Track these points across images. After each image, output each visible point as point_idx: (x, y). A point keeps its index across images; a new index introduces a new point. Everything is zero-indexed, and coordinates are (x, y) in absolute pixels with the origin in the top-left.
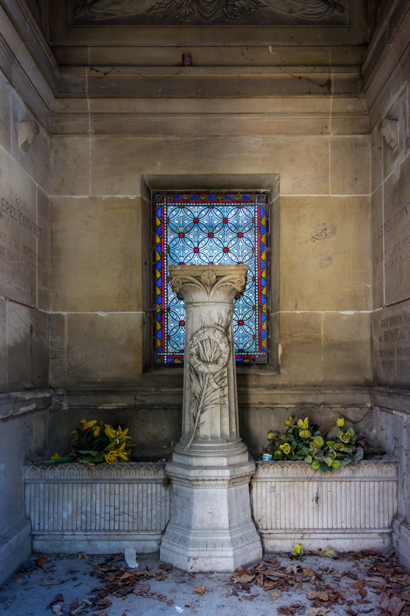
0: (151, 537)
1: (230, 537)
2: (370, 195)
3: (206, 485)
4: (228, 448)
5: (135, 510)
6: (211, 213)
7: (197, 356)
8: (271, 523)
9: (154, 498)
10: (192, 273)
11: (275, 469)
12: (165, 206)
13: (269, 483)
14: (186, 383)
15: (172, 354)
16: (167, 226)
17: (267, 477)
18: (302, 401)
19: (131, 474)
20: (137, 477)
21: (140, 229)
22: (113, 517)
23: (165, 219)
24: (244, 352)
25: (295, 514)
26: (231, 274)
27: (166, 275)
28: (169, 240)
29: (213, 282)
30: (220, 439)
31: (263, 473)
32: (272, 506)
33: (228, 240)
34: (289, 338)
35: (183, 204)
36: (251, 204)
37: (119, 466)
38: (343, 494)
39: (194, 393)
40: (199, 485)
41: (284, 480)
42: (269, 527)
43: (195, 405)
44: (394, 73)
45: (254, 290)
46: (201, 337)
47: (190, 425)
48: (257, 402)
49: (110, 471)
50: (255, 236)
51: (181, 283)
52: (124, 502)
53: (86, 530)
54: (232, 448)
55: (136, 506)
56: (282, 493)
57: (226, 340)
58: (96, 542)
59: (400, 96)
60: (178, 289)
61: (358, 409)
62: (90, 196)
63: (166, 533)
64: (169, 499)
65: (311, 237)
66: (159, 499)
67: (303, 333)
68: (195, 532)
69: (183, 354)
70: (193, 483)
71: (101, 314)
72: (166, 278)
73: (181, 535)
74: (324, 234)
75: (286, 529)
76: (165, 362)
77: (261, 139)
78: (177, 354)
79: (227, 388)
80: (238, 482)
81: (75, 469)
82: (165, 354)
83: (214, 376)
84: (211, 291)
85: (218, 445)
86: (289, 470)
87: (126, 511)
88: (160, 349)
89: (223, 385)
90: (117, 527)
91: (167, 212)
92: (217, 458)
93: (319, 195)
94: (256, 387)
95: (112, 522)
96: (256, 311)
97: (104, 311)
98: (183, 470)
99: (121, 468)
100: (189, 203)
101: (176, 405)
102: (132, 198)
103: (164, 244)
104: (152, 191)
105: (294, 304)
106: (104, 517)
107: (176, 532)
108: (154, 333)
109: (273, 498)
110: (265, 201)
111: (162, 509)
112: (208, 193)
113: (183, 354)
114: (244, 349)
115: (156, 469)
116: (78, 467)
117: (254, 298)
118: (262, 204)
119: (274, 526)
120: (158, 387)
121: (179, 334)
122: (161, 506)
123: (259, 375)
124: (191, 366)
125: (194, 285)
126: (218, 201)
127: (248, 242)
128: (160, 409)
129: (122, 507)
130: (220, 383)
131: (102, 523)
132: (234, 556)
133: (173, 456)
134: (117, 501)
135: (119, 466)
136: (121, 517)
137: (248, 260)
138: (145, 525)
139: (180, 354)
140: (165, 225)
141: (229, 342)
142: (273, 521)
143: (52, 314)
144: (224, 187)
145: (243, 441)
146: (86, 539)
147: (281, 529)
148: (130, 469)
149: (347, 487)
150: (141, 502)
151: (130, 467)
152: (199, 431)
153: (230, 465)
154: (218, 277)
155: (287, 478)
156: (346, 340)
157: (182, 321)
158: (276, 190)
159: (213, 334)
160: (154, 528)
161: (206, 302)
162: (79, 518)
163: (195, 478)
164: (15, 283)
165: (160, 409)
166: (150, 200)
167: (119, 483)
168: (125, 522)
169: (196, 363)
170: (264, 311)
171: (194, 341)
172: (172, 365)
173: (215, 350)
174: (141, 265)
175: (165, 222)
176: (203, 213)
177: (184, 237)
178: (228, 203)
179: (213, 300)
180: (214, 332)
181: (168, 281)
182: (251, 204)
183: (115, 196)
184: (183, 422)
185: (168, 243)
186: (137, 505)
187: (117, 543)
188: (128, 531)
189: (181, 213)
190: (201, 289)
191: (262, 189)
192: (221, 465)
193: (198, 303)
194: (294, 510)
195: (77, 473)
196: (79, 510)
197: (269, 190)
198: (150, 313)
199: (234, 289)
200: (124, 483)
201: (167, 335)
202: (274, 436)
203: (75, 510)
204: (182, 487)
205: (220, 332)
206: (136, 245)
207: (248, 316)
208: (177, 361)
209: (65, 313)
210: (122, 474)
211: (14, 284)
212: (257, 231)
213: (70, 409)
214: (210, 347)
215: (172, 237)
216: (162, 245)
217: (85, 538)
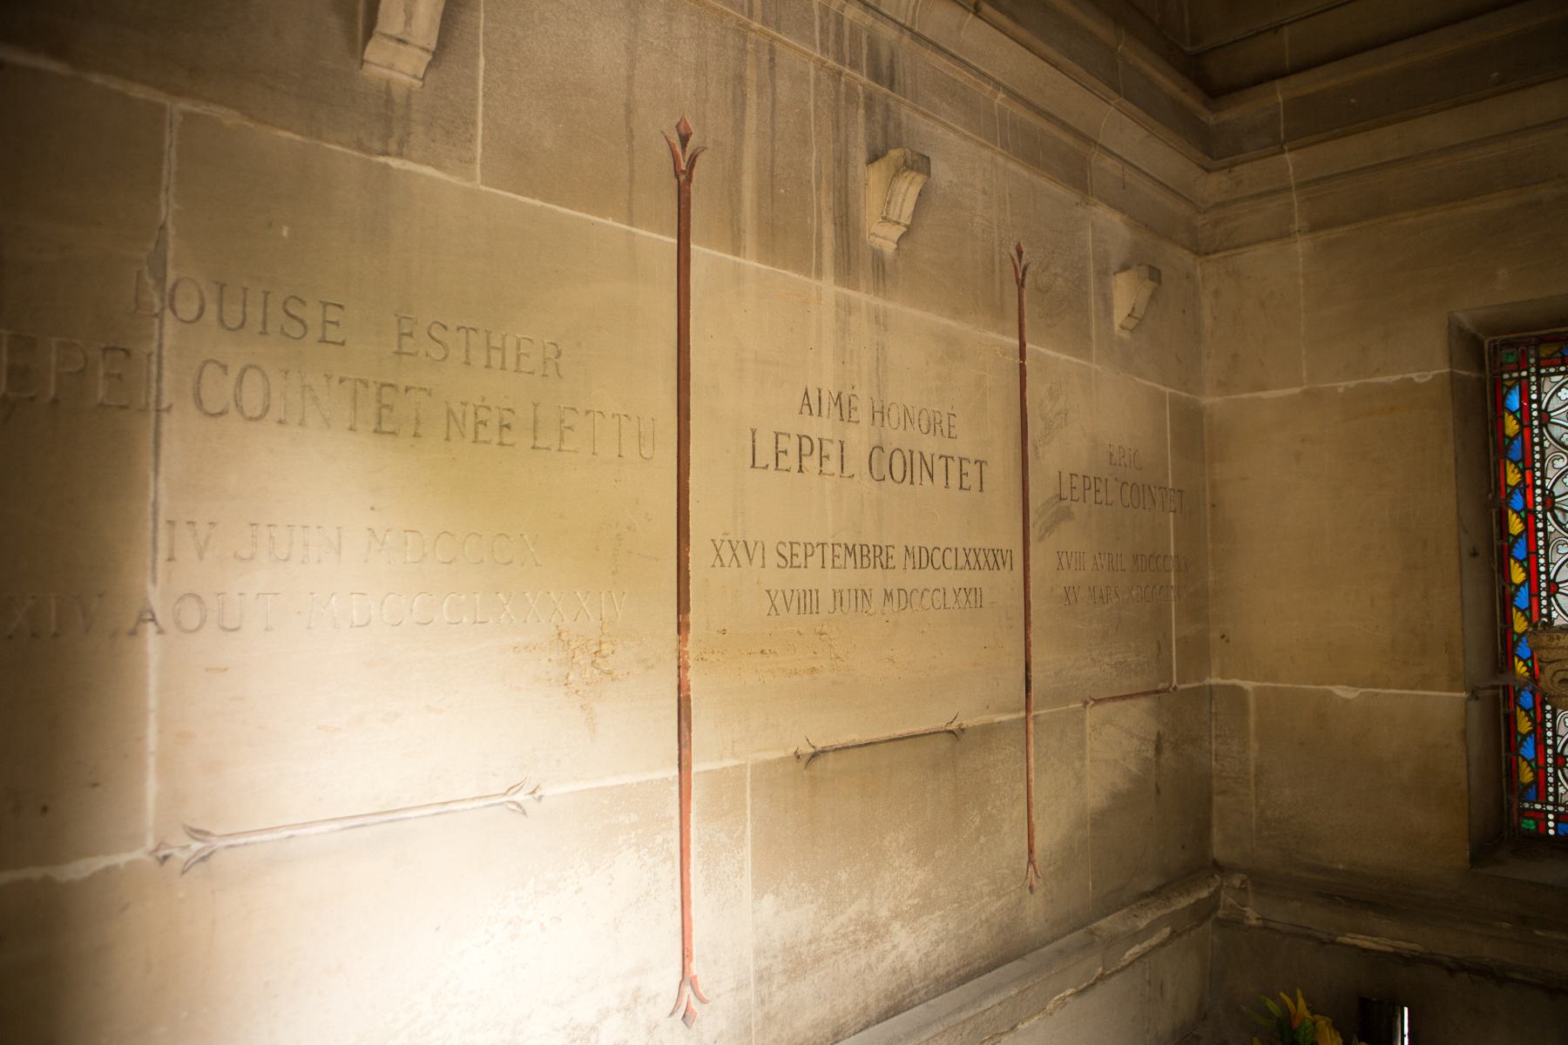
12: (1533, 379)
16: (1541, 435)
23: (1535, 414)
27: (1543, 577)
28: (1551, 473)
71: (1343, 692)
72: (1543, 585)
82: (1550, 808)
88: (1532, 793)
97: (1352, 683)
103: (1536, 487)
104: (1486, 342)
108: (1508, 741)
143: (1218, 686)
164: (1111, 655)
166: (1482, 367)
175: (1536, 423)
183: (1372, 380)
185: (1548, 484)
206: (1441, 504)
209: (1248, 685)
211: (1107, 659)
213: (1265, 928)
215: (1560, 464)
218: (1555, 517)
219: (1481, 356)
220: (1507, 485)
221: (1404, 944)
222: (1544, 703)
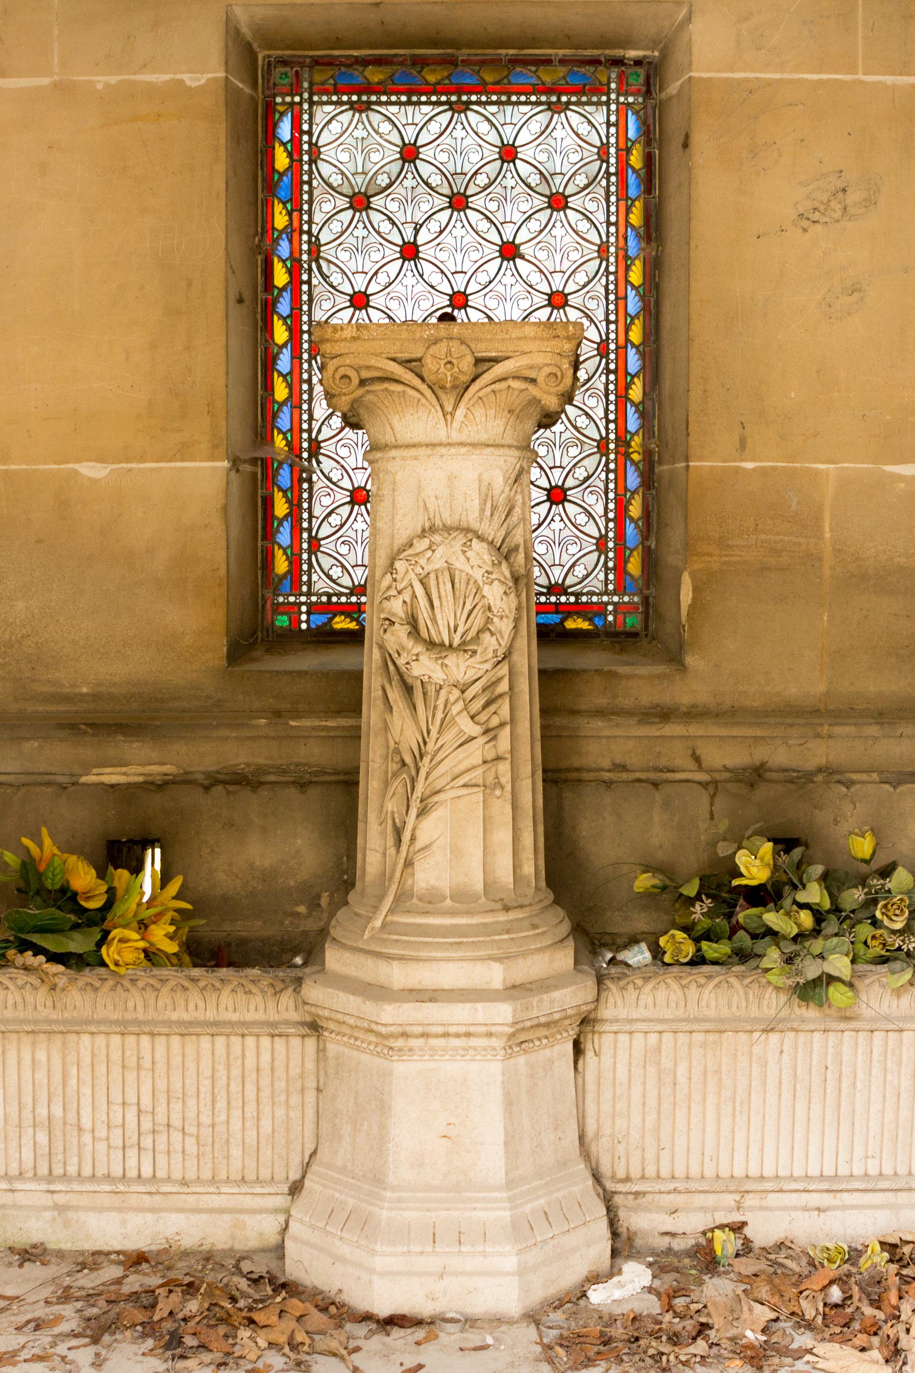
0: (259, 1202)
1: (507, 1213)
3: (432, 1049)
4: (508, 932)
5: (206, 1120)
6: (459, 126)
7: (408, 628)
8: (643, 1159)
9: (265, 1082)
10: (393, 351)
11: (662, 994)
12: (306, 106)
13: (639, 1037)
14: (372, 714)
15: (324, 599)
16: (310, 172)
17: (635, 1017)
18: (757, 760)
19: (191, 1006)
20: (211, 1015)
21: (220, 183)
22: (135, 1139)
23: (306, 147)
24: (566, 593)
25: (718, 1131)
26: (523, 353)
27: (305, 436)
29: (465, 378)
30: (483, 899)
31: (619, 1003)
32: (647, 1109)
33: (518, 218)
34: (717, 552)
35: (364, 98)
36: (595, 99)
37: (152, 981)
38: (874, 1072)
39: (397, 751)
40: (411, 1050)
41: (689, 1027)
42: (635, 1173)
43: (401, 790)
45: (602, 387)
46: (423, 561)
47: (384, 854)
48: (606, 763)
49: (124, 994)
50: (608, 207)
51: (356, 381)
52: (168, 1092)
53: (50, 1177)
54: (522, 930)
55: (209, 1107)
56: (682, 1069)
57: (507, 574)
58: (82, 1216)
60: (344, 402)
62: (56, 78)
63: (304, 1193)
64: (315, 1085)
65: (794, 216)
66: (283, 1084)
67: (763, 537)
68: (396, 1195)
69: (363, 599)
70: (391, 1043)
71: (91, 470)
73: (351, 1201)
74: (838, 207)
75: (688, 1178)
76: (304, 626)
78: (343, 599)
79: (507, 729)
80: (539, 1039)
81: (12, 987)
82: (303, 599)
83: (463, 692)
84: (456, 406)
85: (475, 920)
86: (706, 996)
87: (176, 1121)
88: (287, 583)
89: (495, 721)
90: (147, 1171)
92: (471, 964)
93: (824, 76)
94: (600, 713)
95: (132, 1153)
96: (607, 455)
97: (101, 460)
98: (359, 1000)
99: (158, 986)
100: (385, 93)
101: (337, 773)
102: (194, 84)
103: (301, 232)
104: (260, 56)
105: (736, 438)
106: (108, 1139)
107: (337, 1195)
108: (264, 528)
109: (651, 1083)
110: (644, 89)
111: (292, 1114)
112: (451, 62)
113: (363, 599)
114: (568, 582)
115: (271, 991)
116: (20, 982)
117: (602, 415)
118: (631, 99)
119: (651, 1171)
120: (278, 714)
121: (351, 533)
122: (288, 1107)
123: (613, 675)
124: (388, 660)
125: (399, 388)
127: (583, 226)
128: (286, 783)
129: (161, 1110)
130: (483, 717)
131: (101, 1157)
132: (522, 1271)
133: (328, 954)
134: (146, 1089)
135: (152, 981)
136: (162, 1139)
137: (584, 286)
138: (236, 1165)
139: (354, 599)
140: (306, 167)
141: (516, 580)
142: (650, 1154)
144: (503, 43)
145: (557, 902)
146: (50, 1203)
147: (673, 1177)
148: (185, 989)
149: (890, 1048)
150: (224, 1093)
151: (186, 984)
152: (413, 875)
153: (514, 987)
154: (483, 363)
155: (697, 1020)
156: (902, 560)
157: (360, 489)
158: (679, 57)
159: (464, 552)
160: (265, 1174)
161: (440, 445)
162: (27, 1140)
163: (400, 1029)
165: (286, 783)
166: (254, 85)
167: (152, 1035)
168: (172, 1155)
169: (403, 648)
170: (636, 457)
171: (399, 577)
172: (327, 638)
173: (468, 607)
174: (221, 306)
175: (306, 158)
176: (434, 127)
177: (368, 207)
178: (519, 94)
179: (463, 438)
180: (467, 545)
181: (312, 357)
182: (595, 99)
183: (138, 77)
184: (360, 841)
185: (315, 231)
186: (209, 1103)
187: (149, 1217)
188: (184, 1183)
189: (360, 126)
190: (423, 401)
191: (634, 49)
192: (485, 987)
193: (414, 446)
194: (718, 1120)
195: (19, 999)
196: (27, 1114)
197: (656, 54)
198: (254, 461)
199: (536, 401)
200: (168, 1035)
202: (654, 887)
203: (15, 1116)
204: (355, 1053)
205: (484, 545)
206: (208, 238)
207: (580, 473)
208: (341, 623)
210: (160, 1004)
212: (613, 189)
215: (327, 207)
216: (296, 235)
217: (47, 1200)
218: (319, 268)
219: (255, 69)
220: (274, 229)
221: (156, 769)
222: (301, 481)
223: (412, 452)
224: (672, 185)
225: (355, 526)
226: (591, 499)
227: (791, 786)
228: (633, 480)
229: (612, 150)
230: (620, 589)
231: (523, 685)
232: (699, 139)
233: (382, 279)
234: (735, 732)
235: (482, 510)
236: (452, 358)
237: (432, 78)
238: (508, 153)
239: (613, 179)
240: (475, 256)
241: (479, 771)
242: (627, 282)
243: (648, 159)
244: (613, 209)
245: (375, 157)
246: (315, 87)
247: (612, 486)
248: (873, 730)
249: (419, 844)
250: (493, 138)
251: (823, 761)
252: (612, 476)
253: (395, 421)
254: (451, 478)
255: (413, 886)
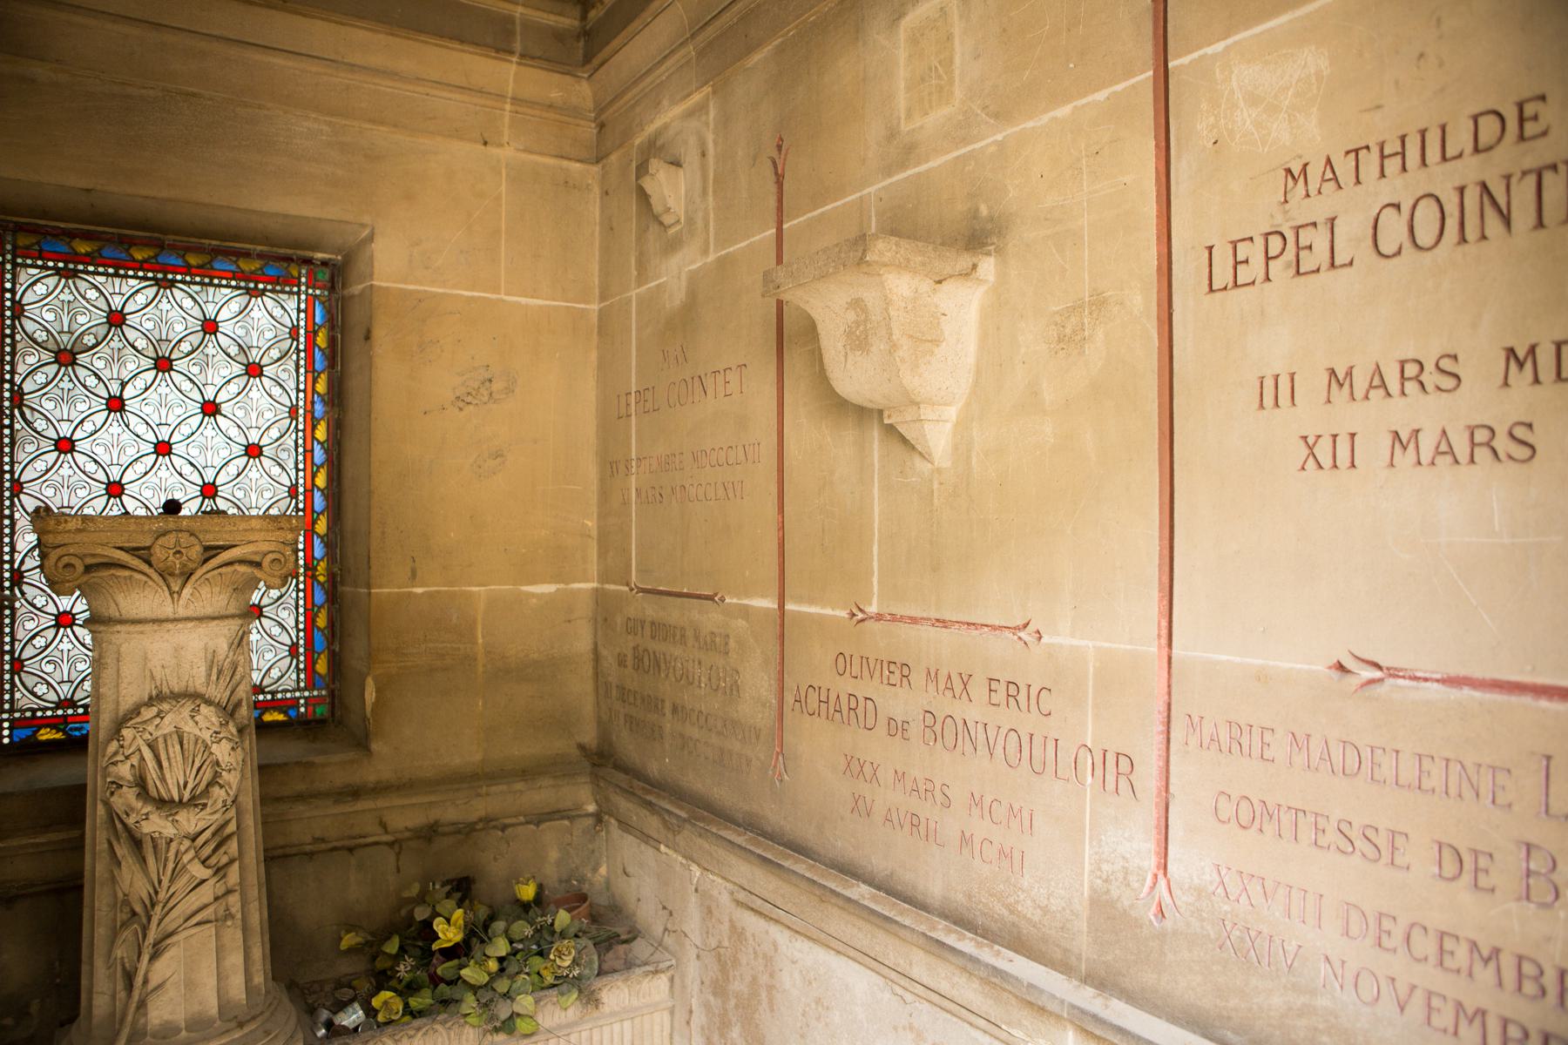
2: (595, 307)
15: (28, 714)
16: (13, 327)
24: (263, 692)
28: (21, 368)
30: (218, 1022)
33: (219, 382)
35: (71, 266)
39: (126, 902)
43: (131, 938)
44: (676, 57)
46: (151, 728)
48: (308, 839)
51: (80, 568)
59: (690, 114)
61: (566, 822)
74: (486, 393)
76: (6, 741)
77: (325, 128)
78: (49, 713)
89: (225, 860)
91: (14, 284)
94: (300, 797)
121: (56, 653)
123: (311, 764)
125: (127, 573)
126: (187, 269)
127: (276, 391)
130: (213, 861)
152: (146, 1015)
154: (211, 551)
156: (536, 656)
169: (132, 809)
171: (126, 744)
173: (197, 764)
179: (190, 613)
180: (196, 710)
184: (84, 982)
201: (12, 657)
212: (302, 362)
214: (179, 758)
215: (31, 360)
218: (23, 415)
223: (139, 628)
224: (354, 366)
225: (61, 646)
226: (284, 614)
227: (460, 837)
228: (319, 597)
229: (302, 331)
230: (310, 685)
231: (250, 821)
232: (379, 333)
233: (88, 427)
234: (414, 800)
235: (209, 675)
236: (182, 544)
237: (138, 256)
238: (210, 327)
239: (302, 355)
240: (179, 411)
241: (211, 909)
242: (314, 438)
243: (332, 341)
244: (302, 379)
245: (81, 319)
246: (18, 251)
247: (301, 602)
248: (519, 786)
249: (151, 986)
250: (196, 312)
251: (482, 813)
252: (301, 594)
253: (120, 598)
254: (178, 650)
255: (146, 1025)
